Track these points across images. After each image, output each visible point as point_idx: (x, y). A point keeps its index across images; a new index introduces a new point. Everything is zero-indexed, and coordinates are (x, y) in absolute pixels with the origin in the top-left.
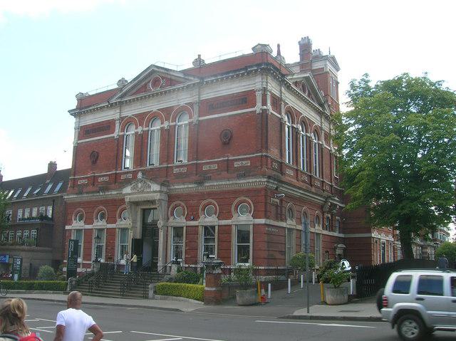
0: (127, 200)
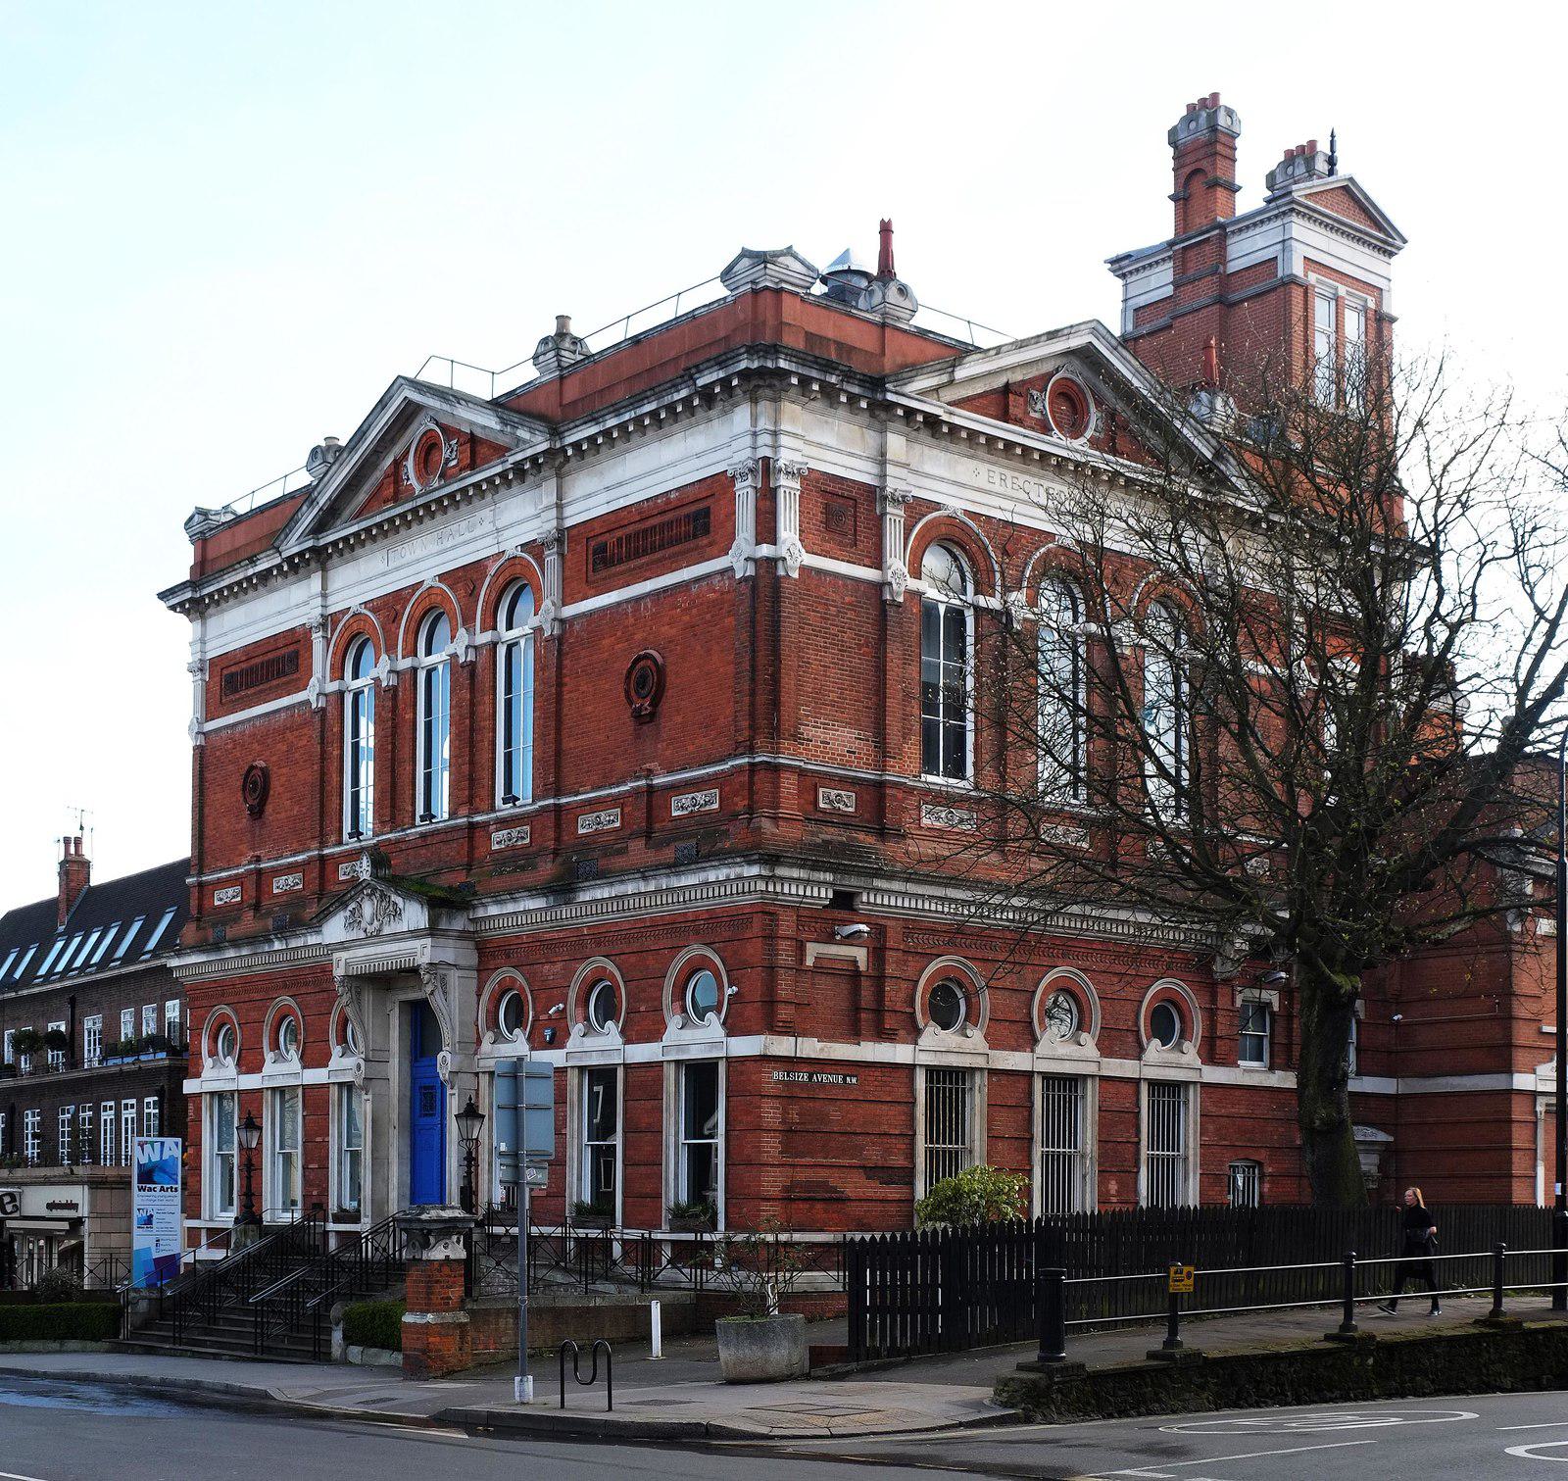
0: (339, 972)
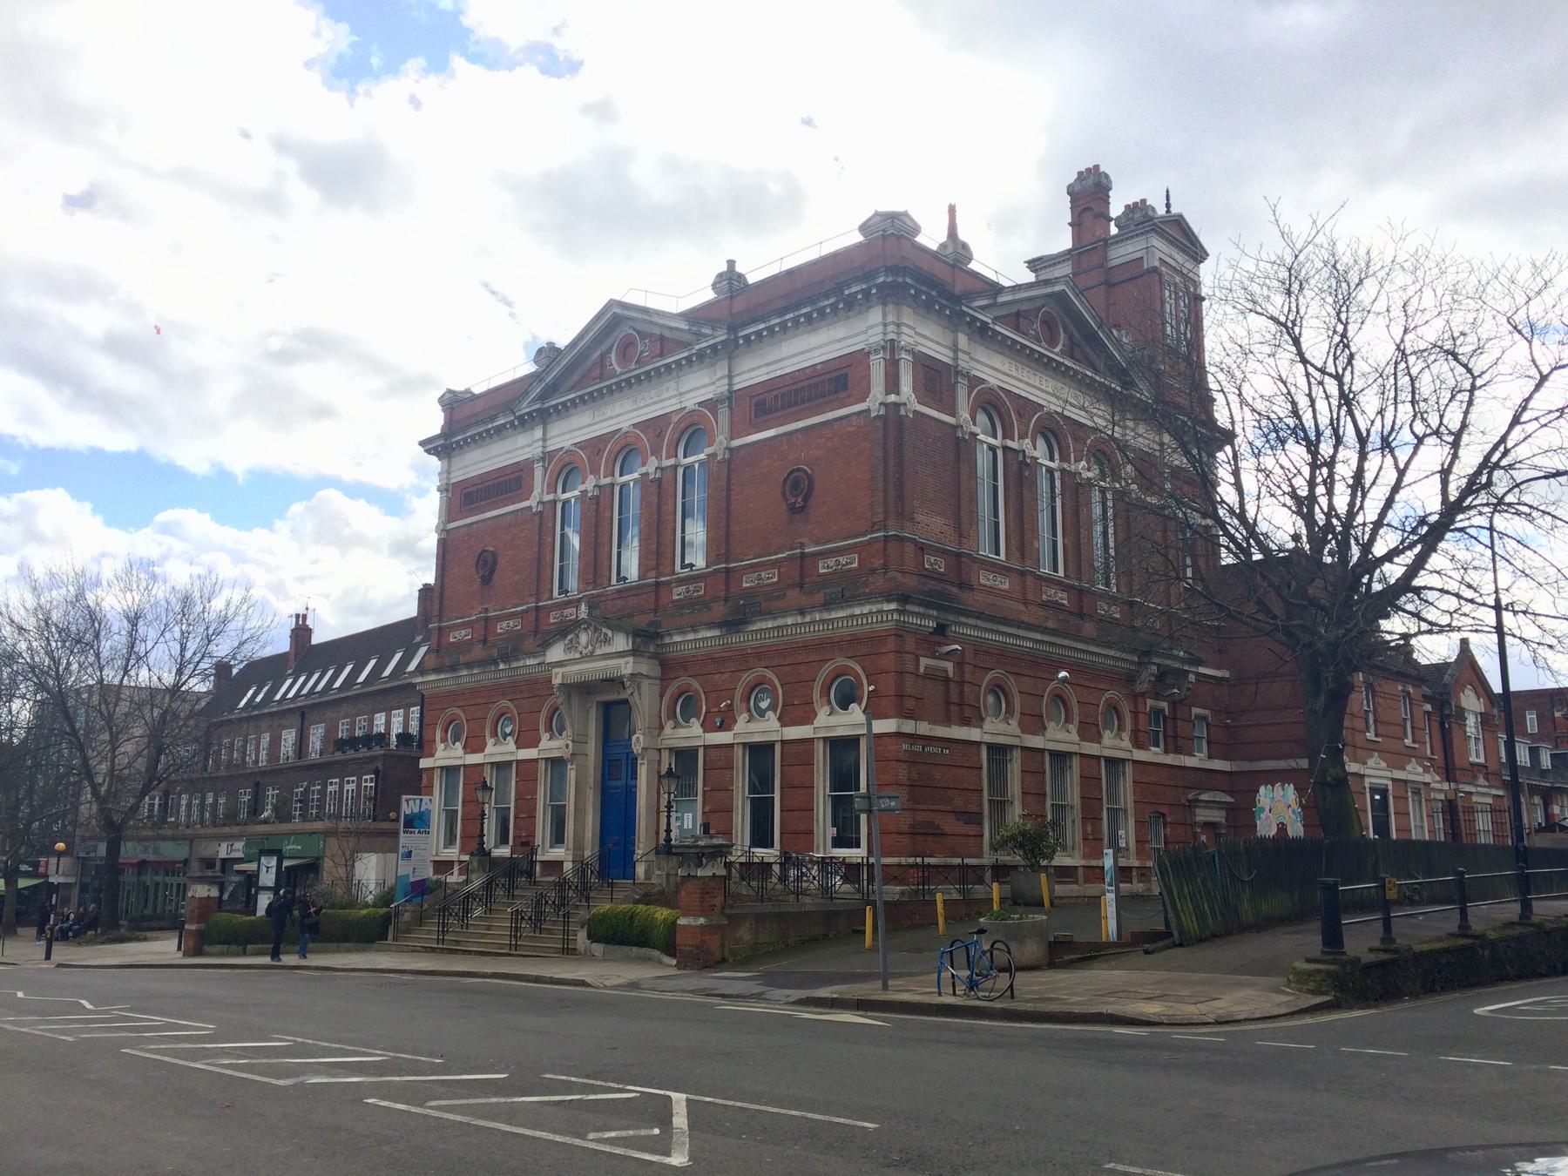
0: (557, 681)
